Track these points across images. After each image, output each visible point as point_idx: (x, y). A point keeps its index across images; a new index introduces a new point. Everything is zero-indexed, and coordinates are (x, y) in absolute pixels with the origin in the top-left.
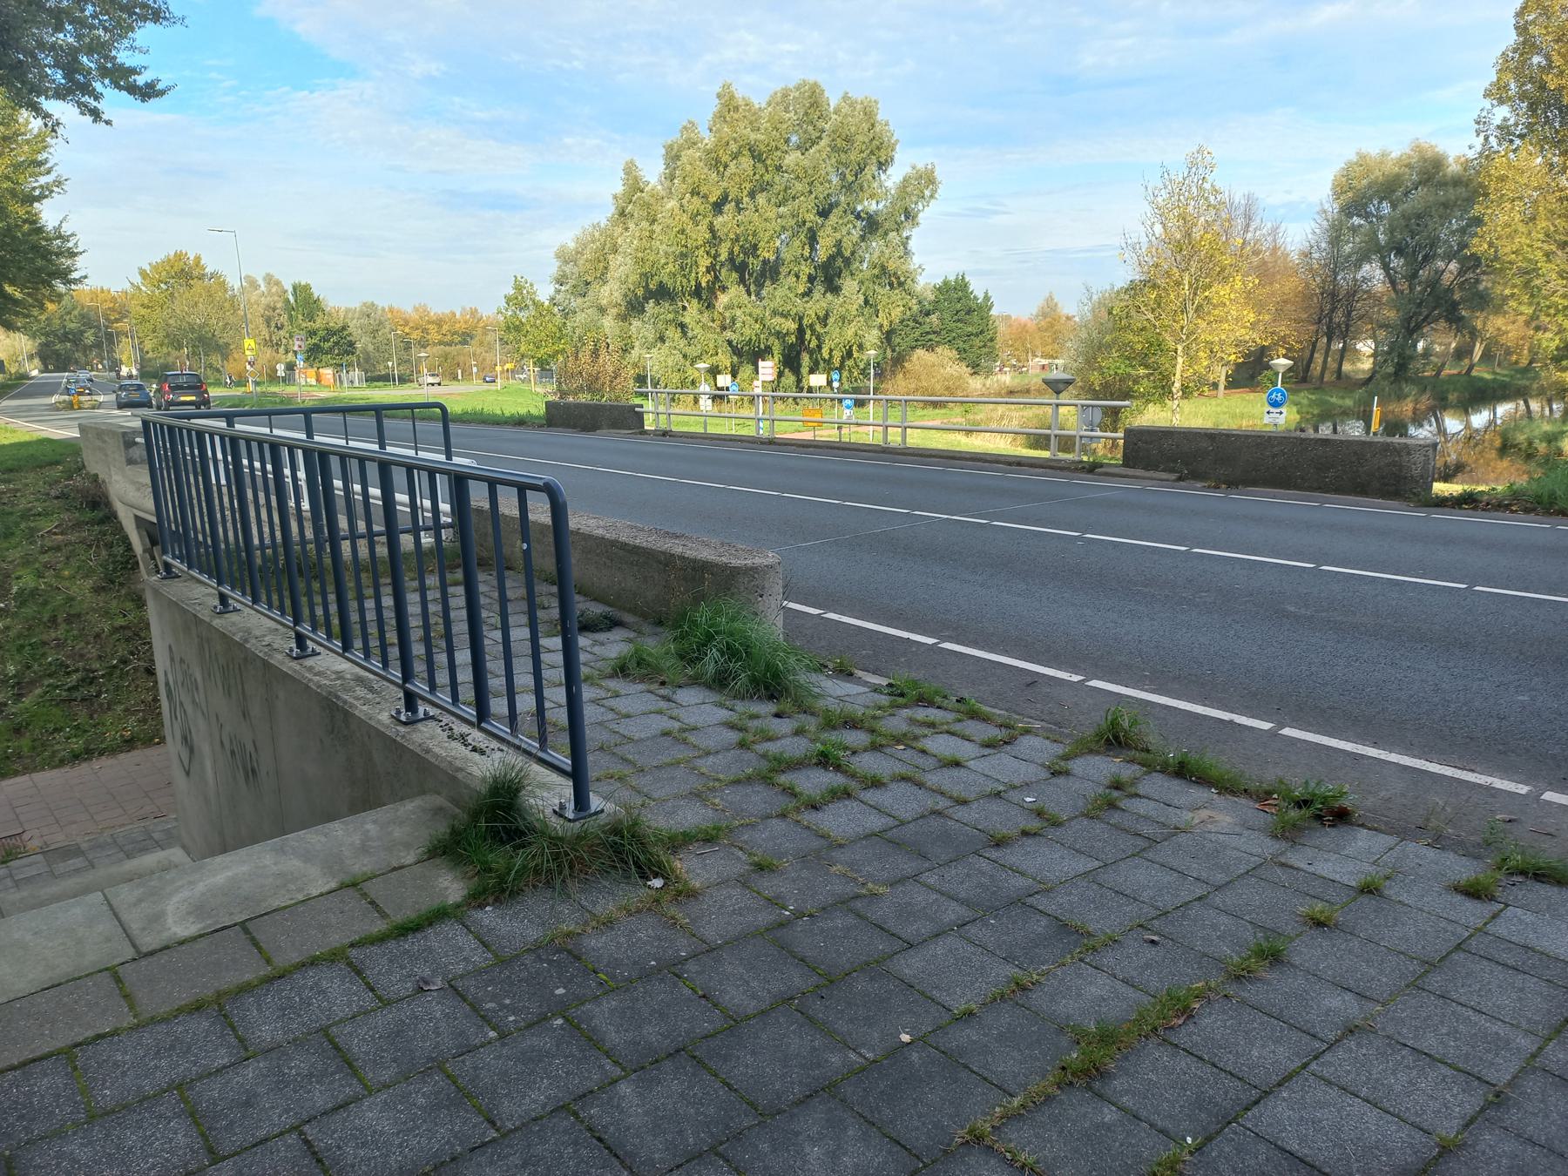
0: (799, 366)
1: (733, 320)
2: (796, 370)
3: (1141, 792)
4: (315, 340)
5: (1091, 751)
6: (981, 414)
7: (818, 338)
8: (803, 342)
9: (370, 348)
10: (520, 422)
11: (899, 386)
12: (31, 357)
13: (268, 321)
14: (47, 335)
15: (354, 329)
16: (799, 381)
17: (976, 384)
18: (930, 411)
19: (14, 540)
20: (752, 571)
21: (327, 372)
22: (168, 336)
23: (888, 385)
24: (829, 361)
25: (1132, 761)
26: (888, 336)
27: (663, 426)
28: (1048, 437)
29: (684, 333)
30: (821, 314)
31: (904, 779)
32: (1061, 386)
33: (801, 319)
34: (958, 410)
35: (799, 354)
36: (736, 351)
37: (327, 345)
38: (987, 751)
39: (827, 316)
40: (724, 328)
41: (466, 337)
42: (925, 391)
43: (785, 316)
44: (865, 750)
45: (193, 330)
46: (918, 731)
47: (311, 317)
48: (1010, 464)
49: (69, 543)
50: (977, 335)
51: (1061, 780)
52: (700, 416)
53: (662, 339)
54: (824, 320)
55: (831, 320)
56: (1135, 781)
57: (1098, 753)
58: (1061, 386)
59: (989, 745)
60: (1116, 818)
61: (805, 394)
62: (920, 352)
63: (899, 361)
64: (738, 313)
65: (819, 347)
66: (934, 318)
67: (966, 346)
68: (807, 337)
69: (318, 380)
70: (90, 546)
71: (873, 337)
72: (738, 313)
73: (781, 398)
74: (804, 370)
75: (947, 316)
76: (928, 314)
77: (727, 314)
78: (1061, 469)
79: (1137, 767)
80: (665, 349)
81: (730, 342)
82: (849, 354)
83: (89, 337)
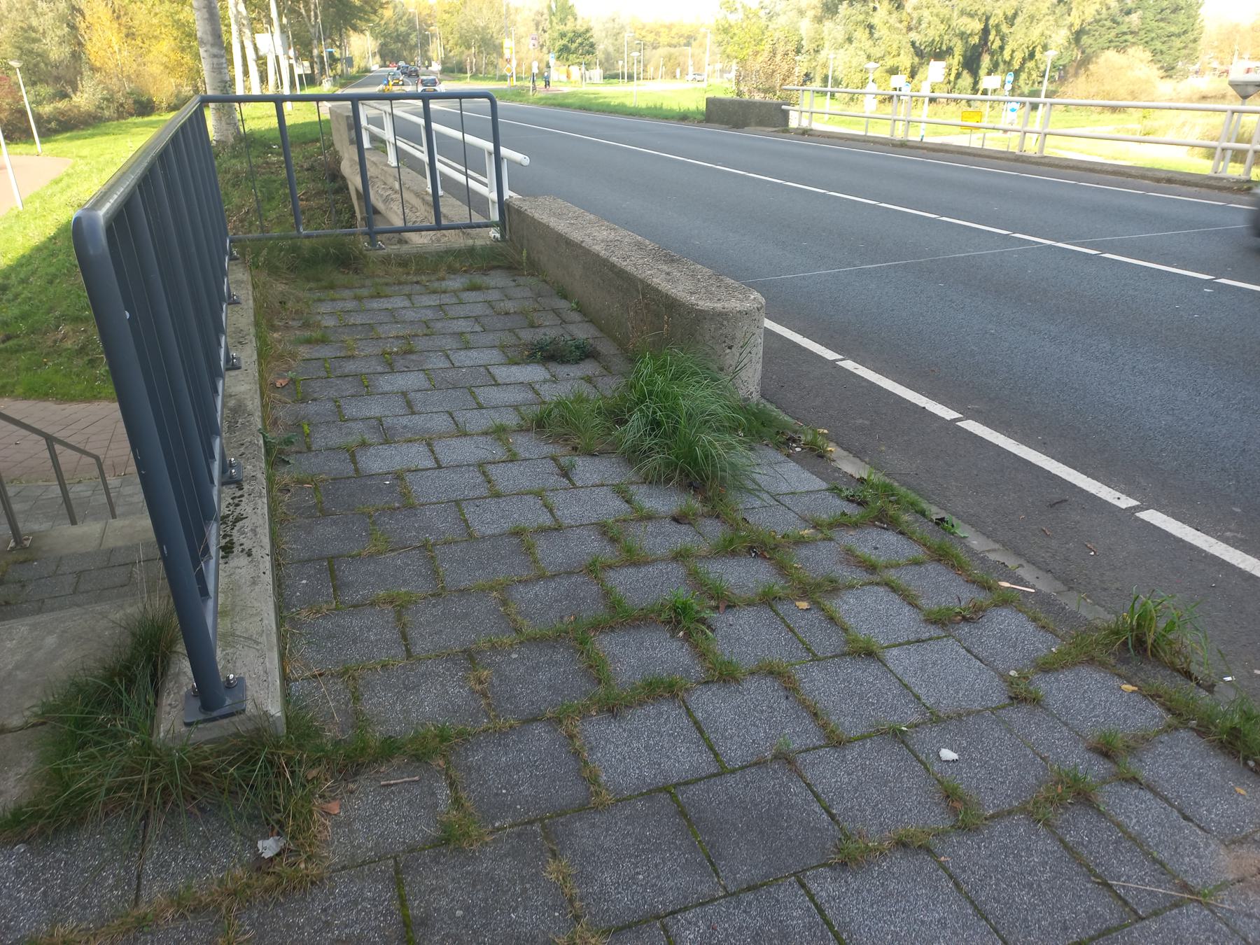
0: (979, 67)
1: (920, 21)
2: (974, 73)
3: (1144, 774)
4: (565, 41)
5: (1091, 661)
6: (1159, 120)
7: (1002, 39)
8: (986, 44)
9: (611, 49)
10: (684, 117)
11: (1078, 89)
12: (374, 55)
13: (537, 25)
14: (385, 36)
15: (597, 35)
16: (976, 83)
17: (1166, 89)
18: (1108, 116)
19: (274, 204)
20: (721, 317)
21: (575, 70)
22: (461, 37)
23: (1068, 88)
24: (1009, 63)
25: (1154, 696)
26: (1078, 35)
27: (805, 124)
28: (1244, 152)
29: (871, 34)
30: (1010, 14)
31: (772, 672)
32: (1250, 89)
33: (988, 19)
34: (1137, 114)
35: (980, 55)
36: (919, 53)
37: (574, 46)
38: (934, 631)
39: (1015, 15)
40: (909, 29)
41: (689, 40)
42: (1107, 95)
43: (971, 16)
44: (750, 604)
45: (477, 32)
46: (846, 574)
47: (563, 21)
48: (1158, 180)
49: (311, 209)
50: (1179, 35)
51: (1017, 715)
52: (866, 118)
53: (850, 40)
54: (1011, 20)
55: (1019, 20)
56: (1141, 743)
57: (1103, 665)
58: (1250, 89)
59: (941, 620)
60: (1080, 829)
61: (979, 96)
62: (1111, 54)
63: (1085, 62)
64: (926, 13)
65: (1002, 48)
66: (1134, 18)
67: (1164, 48)
68: (991, 37)
69: (568, 77)
70: (325, 212)
71: (1060, 37)
72: (926, 13)
73: (955, 100)
74: (983, 72)
75: (1150, 15)
76: (1128, 13)
77: (915, 15)
78: (1220, 189)
79: (1158, 711)
80: (851, 48)
81: (913, 44)
82: (1032, 55)
83: (413, 39)
